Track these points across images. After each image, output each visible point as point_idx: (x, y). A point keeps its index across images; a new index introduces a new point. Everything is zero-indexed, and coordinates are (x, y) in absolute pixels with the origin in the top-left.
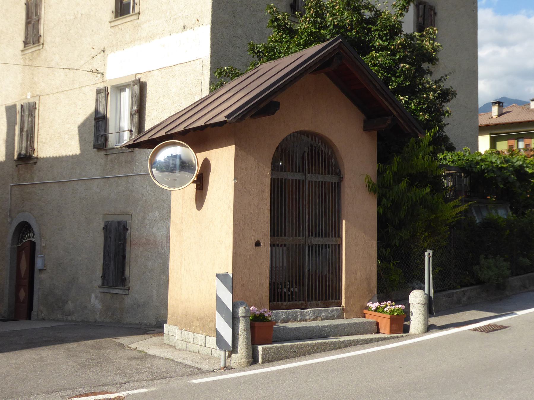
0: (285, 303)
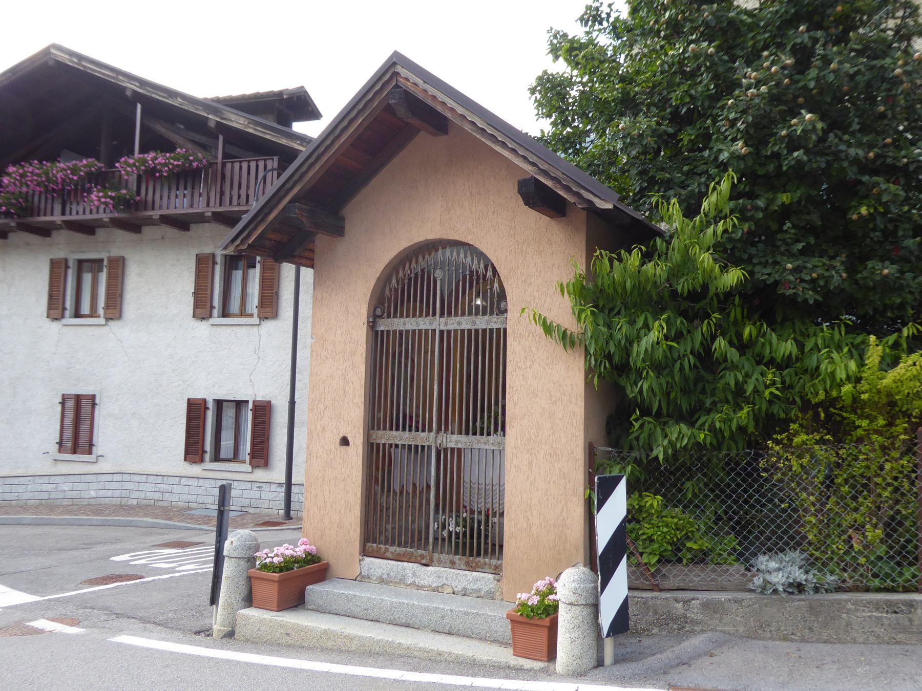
0: (392, 549)
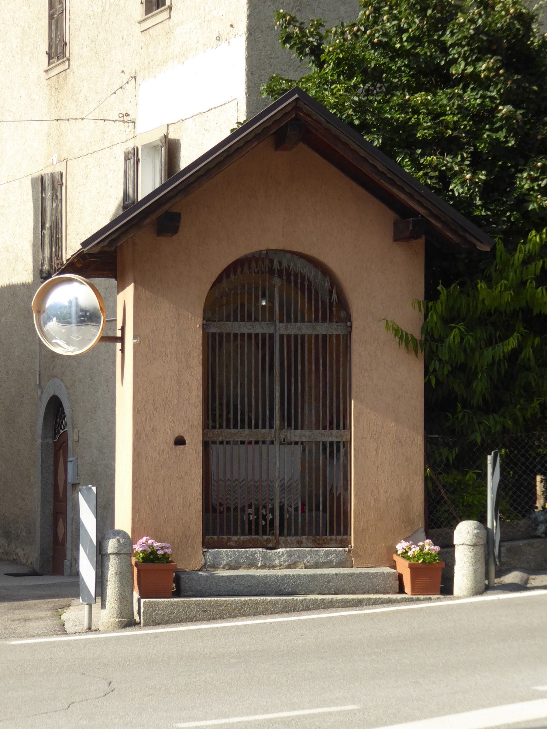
0: (235, 538)
